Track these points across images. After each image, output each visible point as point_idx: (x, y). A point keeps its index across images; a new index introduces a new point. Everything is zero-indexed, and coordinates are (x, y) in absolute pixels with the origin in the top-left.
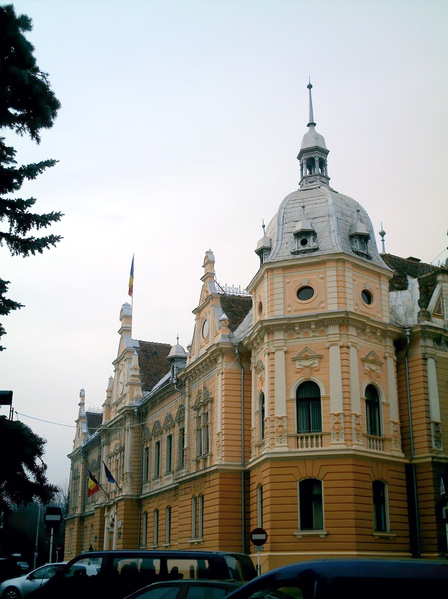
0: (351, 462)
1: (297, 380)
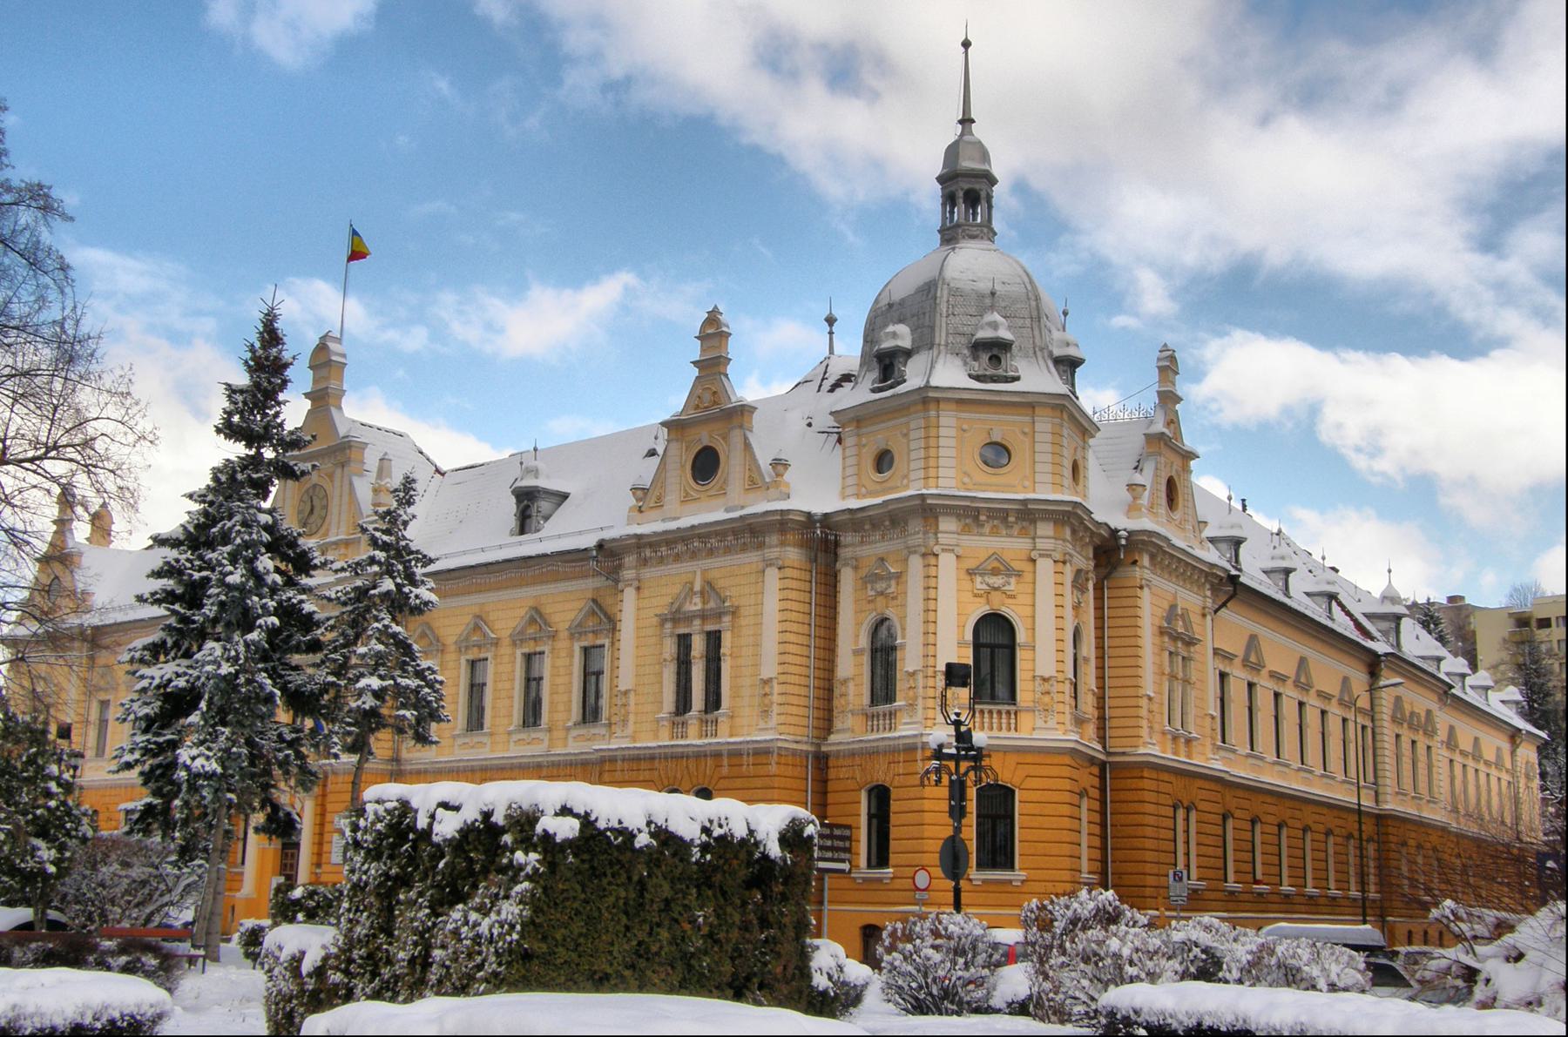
0: (1067, 760)
1: (983, 609)
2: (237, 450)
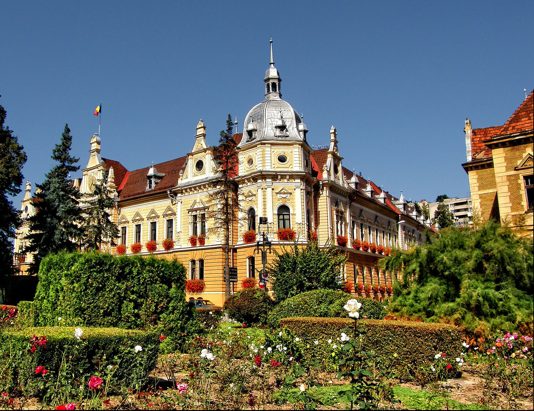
2: (58, 163)
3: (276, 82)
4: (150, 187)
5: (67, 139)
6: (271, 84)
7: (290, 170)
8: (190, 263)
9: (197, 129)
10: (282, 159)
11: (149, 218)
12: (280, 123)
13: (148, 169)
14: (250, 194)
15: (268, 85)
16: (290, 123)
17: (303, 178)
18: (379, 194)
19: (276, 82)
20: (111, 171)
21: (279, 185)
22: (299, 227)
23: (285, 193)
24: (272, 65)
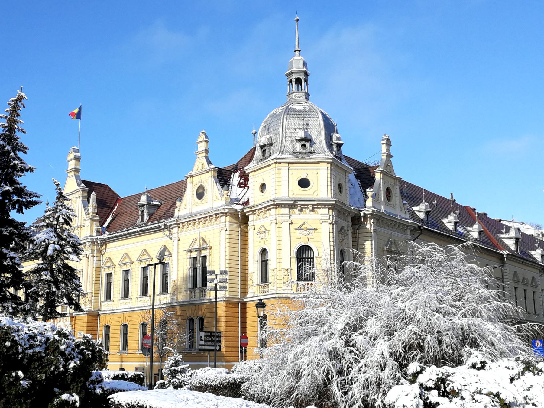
3: (302, 77)
4: (142, 220)
5: (15, 111)
6: (294, 80)
7: (315, 197)
8: (188, 322)
9: (198, 143)
10: (304, 183)
11: (140, 261)
12: (301, 134)
13: (139, 196)
14: (263, 229)
15: (291, 81)
16: (316, 133)
17: (332, 207)
18: (472, 226)
19: (302, 77)
20: (93, 195)
21: (298, 218)
22: (286, 273)
23: (306, 229)
24: (297, 52)
